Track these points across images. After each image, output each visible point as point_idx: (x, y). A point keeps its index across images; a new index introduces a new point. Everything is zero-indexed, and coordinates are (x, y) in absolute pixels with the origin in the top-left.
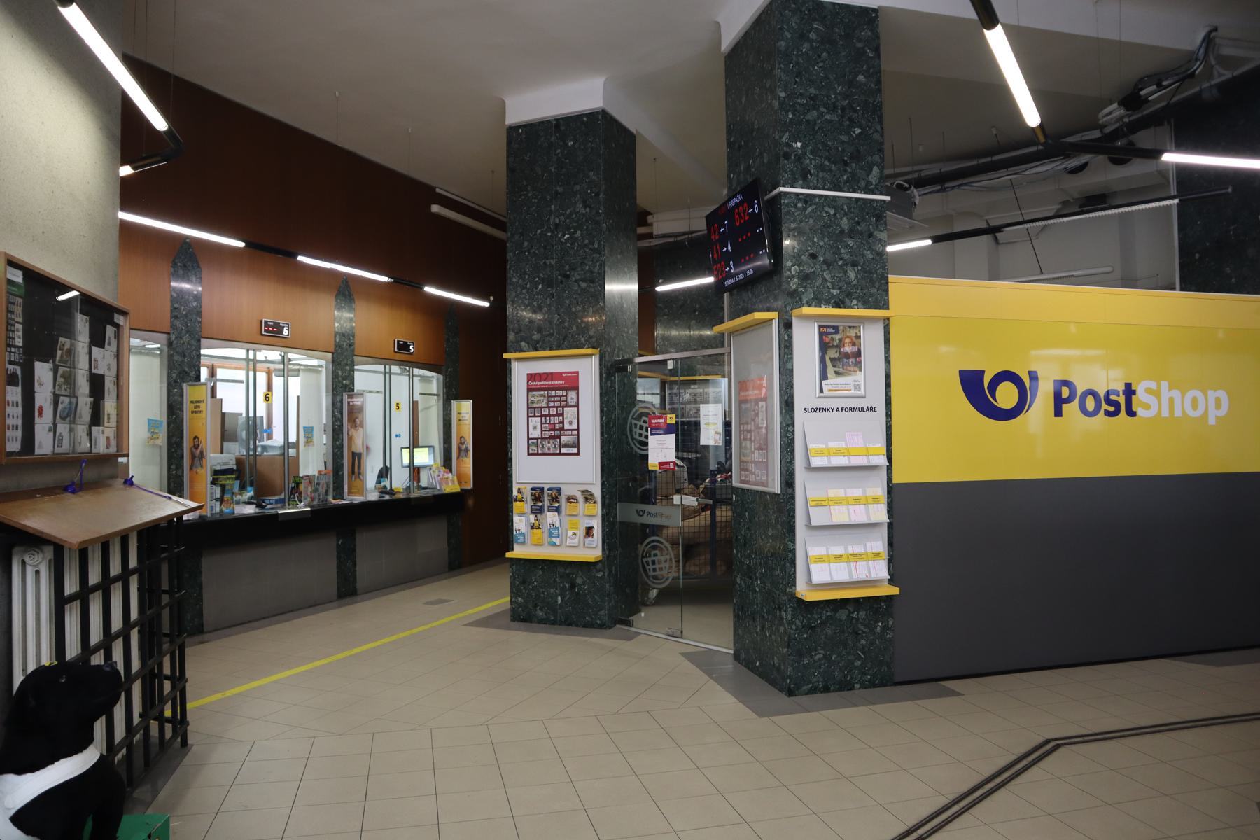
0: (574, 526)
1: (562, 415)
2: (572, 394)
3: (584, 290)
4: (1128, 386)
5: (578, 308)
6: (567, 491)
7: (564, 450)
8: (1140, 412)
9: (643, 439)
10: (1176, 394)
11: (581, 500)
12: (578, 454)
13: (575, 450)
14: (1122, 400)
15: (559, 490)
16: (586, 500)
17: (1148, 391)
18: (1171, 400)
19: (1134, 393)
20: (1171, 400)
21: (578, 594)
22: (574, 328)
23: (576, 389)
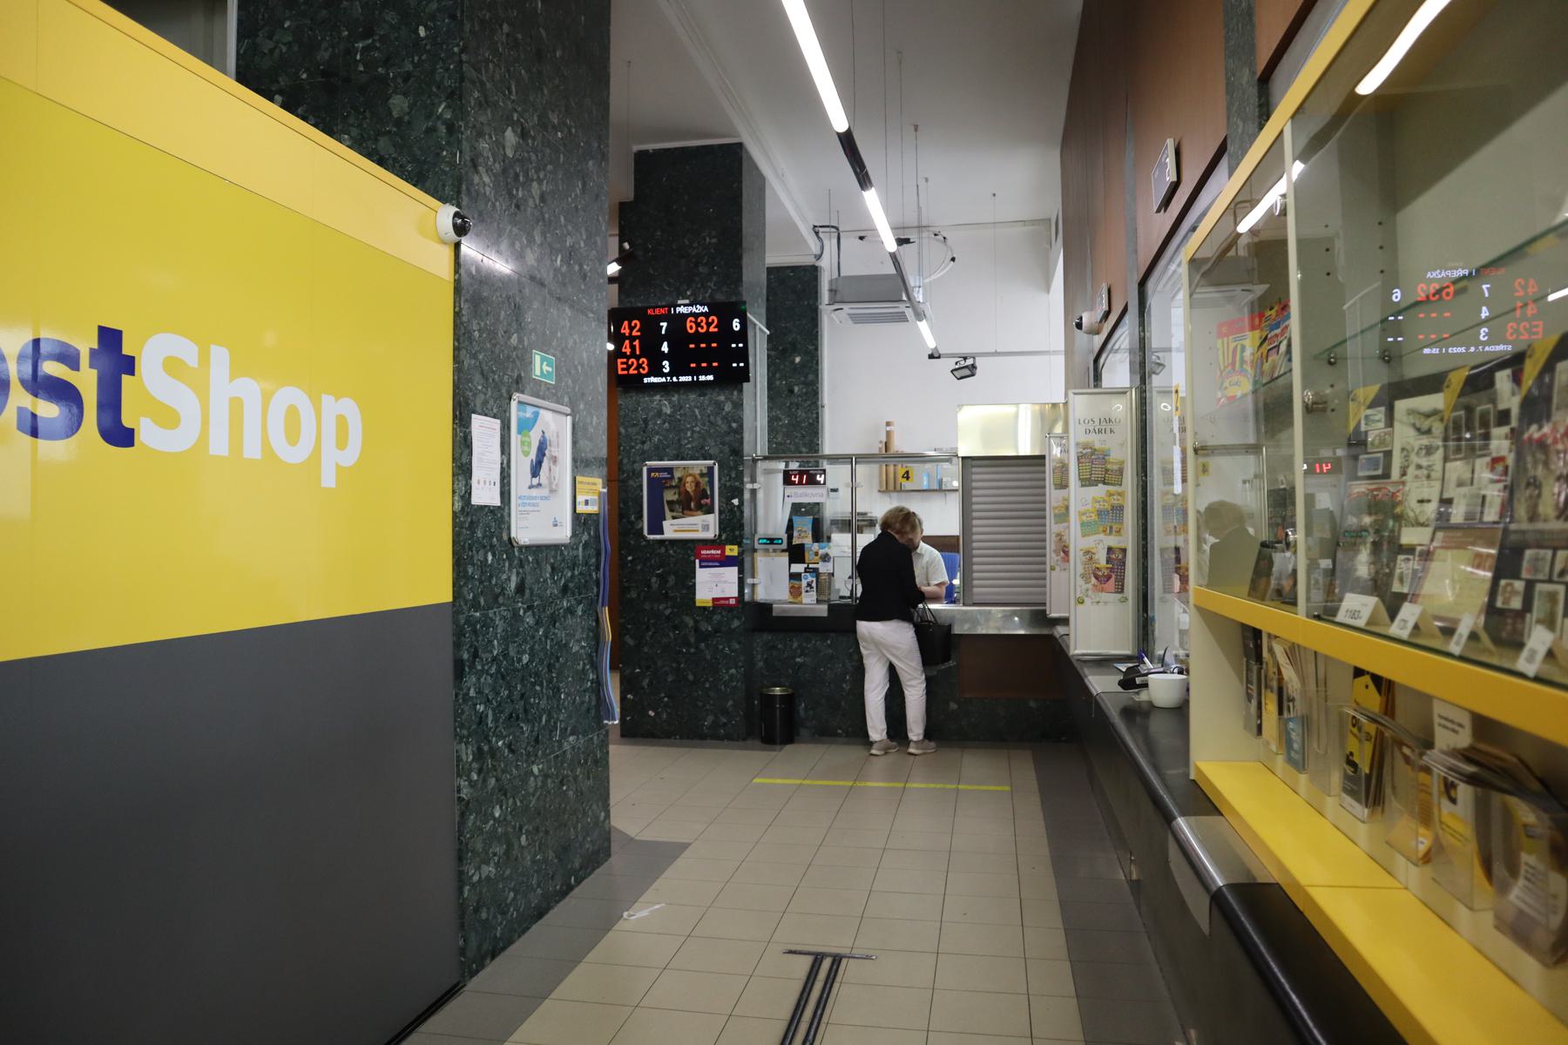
4: (110, 338)
8: (147, 432)
10: (249, 389)
14: (86, 381)
17: (173, 366)
18: (236, 405)
19: (129, 365)
20: (236, 405)
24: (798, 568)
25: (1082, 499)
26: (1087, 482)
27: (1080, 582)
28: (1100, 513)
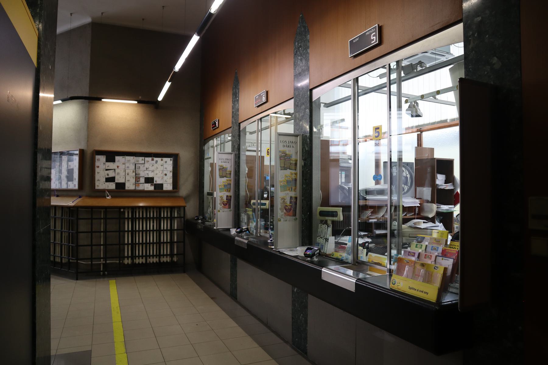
24: (282, 220)
25: (220, 182)
26: (221, 177)
27: (219, 205)
28: (225, 186)
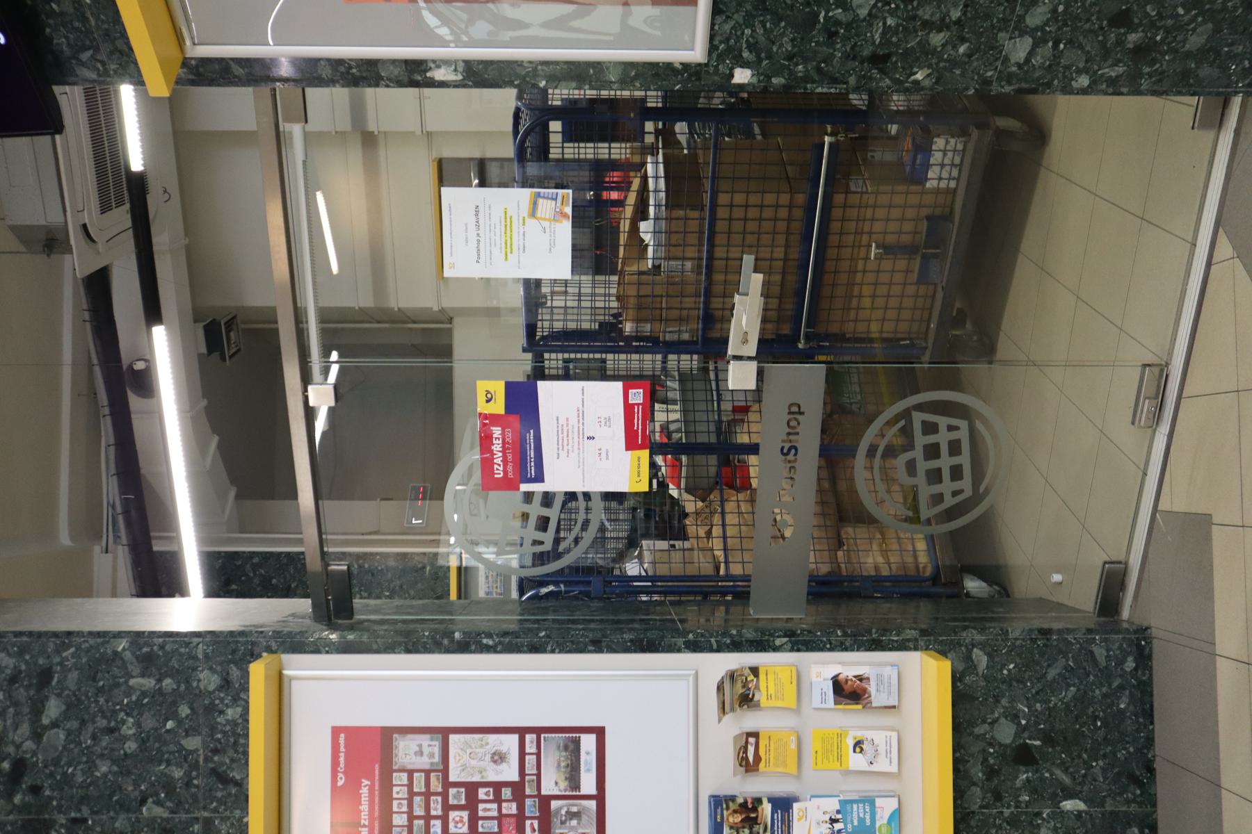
0: (833, 749)
1: (472, 788)
2: (408, 752)
3: (73, 707)
5: (128, 729)
6: (724, 777)
7: (588, 784)
9: (553, 513)
11: (750, 720)
12: (600, 732)
13: (588, 743)
15: (718, 802)
16: (746, 700)
21: (1048, 739)
22: (193, 743)
23: (387, 735)
